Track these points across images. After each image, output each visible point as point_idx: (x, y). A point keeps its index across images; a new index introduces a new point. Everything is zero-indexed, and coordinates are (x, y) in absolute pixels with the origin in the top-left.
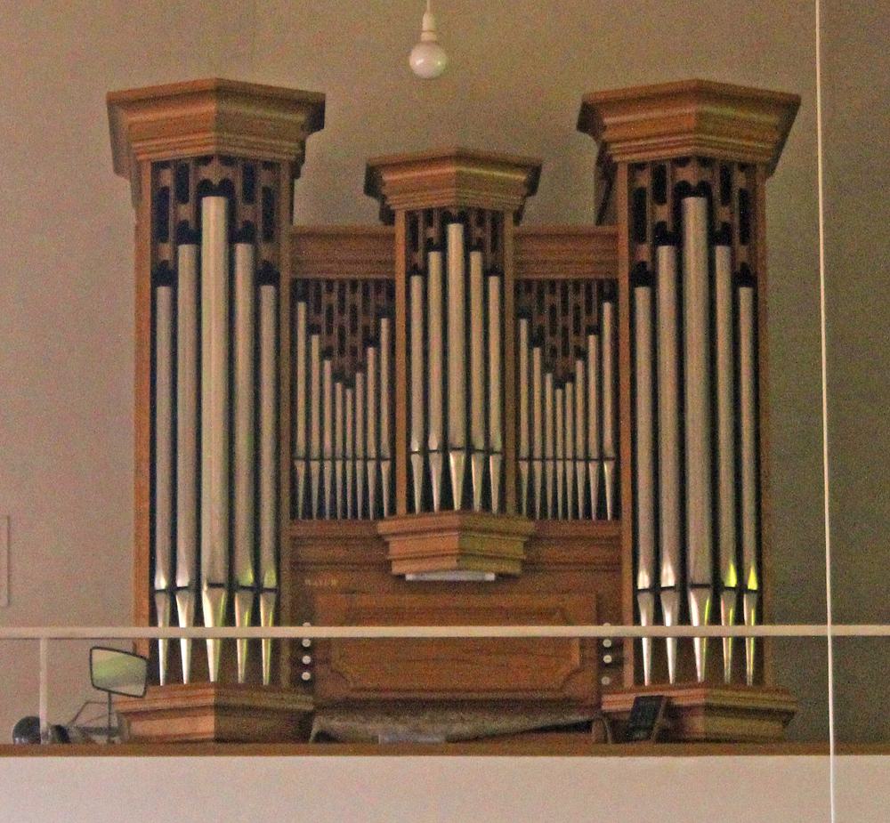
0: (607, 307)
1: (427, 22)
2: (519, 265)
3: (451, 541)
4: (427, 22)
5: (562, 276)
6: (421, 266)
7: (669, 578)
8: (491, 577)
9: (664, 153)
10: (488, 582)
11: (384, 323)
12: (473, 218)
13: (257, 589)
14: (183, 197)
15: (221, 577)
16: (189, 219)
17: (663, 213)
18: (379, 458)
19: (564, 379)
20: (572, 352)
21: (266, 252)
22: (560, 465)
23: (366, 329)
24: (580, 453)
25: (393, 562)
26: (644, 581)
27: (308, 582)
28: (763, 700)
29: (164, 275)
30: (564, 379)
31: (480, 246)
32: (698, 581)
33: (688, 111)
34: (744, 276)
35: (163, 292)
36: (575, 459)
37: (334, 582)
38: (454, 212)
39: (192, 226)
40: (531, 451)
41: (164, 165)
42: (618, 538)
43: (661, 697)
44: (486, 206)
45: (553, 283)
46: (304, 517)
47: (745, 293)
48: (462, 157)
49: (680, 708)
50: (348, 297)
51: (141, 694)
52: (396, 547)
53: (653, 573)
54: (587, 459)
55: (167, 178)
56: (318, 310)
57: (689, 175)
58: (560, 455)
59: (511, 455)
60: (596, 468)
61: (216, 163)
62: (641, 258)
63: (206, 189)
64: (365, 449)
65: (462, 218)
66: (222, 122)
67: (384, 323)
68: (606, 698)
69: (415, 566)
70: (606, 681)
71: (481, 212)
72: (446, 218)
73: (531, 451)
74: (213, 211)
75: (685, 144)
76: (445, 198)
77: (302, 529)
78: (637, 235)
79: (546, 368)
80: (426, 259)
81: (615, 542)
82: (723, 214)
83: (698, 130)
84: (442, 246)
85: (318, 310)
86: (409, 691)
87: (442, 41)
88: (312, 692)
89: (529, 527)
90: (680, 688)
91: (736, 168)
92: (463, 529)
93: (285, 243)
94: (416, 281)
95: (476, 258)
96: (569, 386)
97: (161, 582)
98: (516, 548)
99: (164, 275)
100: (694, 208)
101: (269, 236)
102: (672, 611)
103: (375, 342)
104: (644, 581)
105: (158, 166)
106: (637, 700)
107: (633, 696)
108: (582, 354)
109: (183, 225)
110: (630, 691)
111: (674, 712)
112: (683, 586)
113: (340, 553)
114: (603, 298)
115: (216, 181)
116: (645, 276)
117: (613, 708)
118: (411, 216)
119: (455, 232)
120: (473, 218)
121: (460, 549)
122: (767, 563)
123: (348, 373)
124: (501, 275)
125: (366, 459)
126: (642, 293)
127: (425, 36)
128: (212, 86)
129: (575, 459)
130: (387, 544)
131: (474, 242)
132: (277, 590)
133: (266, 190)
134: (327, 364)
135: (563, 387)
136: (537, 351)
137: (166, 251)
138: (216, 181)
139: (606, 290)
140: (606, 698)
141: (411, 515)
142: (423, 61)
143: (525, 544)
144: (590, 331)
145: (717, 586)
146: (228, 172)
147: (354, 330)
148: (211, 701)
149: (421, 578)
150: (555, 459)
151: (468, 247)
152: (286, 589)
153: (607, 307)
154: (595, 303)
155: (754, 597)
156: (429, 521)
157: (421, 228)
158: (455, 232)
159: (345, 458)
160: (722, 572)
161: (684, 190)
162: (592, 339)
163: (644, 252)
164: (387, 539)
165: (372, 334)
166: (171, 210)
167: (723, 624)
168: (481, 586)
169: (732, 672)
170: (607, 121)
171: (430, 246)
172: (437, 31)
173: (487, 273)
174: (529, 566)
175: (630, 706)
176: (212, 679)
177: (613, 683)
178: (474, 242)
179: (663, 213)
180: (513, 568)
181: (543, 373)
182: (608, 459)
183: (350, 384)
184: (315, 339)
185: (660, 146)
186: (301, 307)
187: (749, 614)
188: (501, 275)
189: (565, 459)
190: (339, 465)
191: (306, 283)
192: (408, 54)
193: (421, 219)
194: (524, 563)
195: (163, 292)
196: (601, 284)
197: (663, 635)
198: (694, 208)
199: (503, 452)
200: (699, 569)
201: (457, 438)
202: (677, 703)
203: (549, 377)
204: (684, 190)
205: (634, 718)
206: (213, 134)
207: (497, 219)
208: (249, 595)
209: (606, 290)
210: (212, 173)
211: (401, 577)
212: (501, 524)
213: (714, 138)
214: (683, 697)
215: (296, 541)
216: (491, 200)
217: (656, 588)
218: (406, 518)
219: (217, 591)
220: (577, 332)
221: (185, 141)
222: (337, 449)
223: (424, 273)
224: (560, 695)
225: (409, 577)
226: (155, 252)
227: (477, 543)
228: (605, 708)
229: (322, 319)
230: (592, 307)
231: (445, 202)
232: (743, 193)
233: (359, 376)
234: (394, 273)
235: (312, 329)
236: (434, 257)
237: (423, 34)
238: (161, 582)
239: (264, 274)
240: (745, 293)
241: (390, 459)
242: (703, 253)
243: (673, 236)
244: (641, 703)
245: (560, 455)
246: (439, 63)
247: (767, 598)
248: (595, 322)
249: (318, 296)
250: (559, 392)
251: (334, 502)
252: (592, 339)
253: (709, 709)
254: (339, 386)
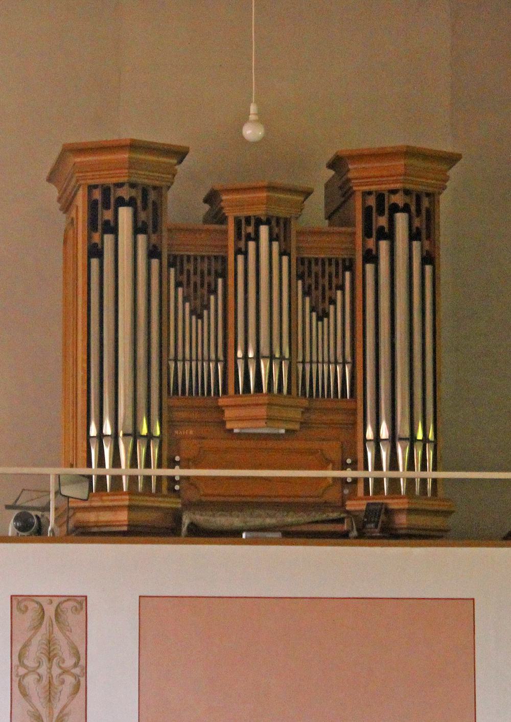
0: (348, 274)
1: (253, 108)
2: (298, 248)
3: (262, 412)
4: (253, 108)
5: (323, 256)
6: (243, 249)
7: (384, 433)
8: (283, 431)
9: (383, 187)
10: (282, 434)
11: (220, 281)
12: (274, 223)
13: (150, 436)
14: (106, 206)
15: (130, 431)
16: (110, 219)
17: (383, 221)
18: (217, 361)
19: (323, 315)
20: (327, 302)
21: (154, 238)
22: (320, 366)
23: (209, 285)
24: (332, 359)
25: (227, 422)
26: (370, 434)
27: (176, 432)
28: (435, 505)
29: (95, 251)
30: (323, 315)
31: (277, 239)
32: (402, 436)
33: (399, 164)
34: (428, 259)
35: (95, 262)
36: (329, 362)
37: (191, 432)
38: (264, 218)
39: (112, 224)
40: (191, 357)
41: (96, 187)
42: (355, 410)
43: (383, 503)
44: (281, 215)
45: (316, 260)
46: (173, 394)
47: (428, 268)
48: (271, 188)
49: (392, 510)
50: (199, 265)
51: (86, 498)
52: (228, 413)
53: (375, 430)
54: (336, 363)
55: (97, 195)
56: (182, 273)
57: (398, 199)
58: (320, 360)
59: (294, 361)
60: (213, 365)
61: (126, 187)
62: (368, 247)
63: (121, 202)
64: (323, 359)
65: (268, 222)
66: (132, 165)
67: (220, 281)
68: (348, 503)
69: (241, 425)
70: (346, 491)
71: (278, 219)
72: (259, 222)
73: (191, 357)
74: (125, 215)
75: (396, 182)
76: (260, 211)
77: (175, 402)
78: (367, 233)
79: (312, 309)
80: (246, 246)
81: (354, 412)
82: (417, 223)
83: (405, 175)
84: (257, 239)
85: (182, 273)
86: (270, 497)
87: (263, 119)
88: (179, 497)
89: (305, 403)
90: (393, 498)
91: (424, 194)
92: (270, 405)
93: (165, 234)
94: (240, 258)
95: (275, 245)
96: (326, 320)
97: (93, 432)
98: (296, 414)
99: (95, 251)
100: (401, 219)
101: (156, 228)
102: (387, 450)
103: (215, 292)
104: (370, 434)
105: (91, 188)
106: (368, 505)
107: (365, 502)
108: (333, 302)
109: (107, 223)
110: (361, 499)
111: (389, 512)
112: (393, 439)
113: (195, 416)
114: (346, 269)
115: (127, 198)
116: (371, 257)
117: (353, 508)
118: (238, 222)
119: (264, 230)
120: (274, 223)
121: (267, 416)
122: (439, 426)
123: (199, 312)
124: (289, 255)
125: (209, 360)
126: (370, 267)
127: (252, 117)
128: (128, 142)
129: (329, 362)
130: (223, 412)
131: (275, 236)
132: (160, 438)
133: (154, 203)
134: (187, 305)
135: (322, 320)
136: (307, 299)
137: (96, 238)
138: (127, 198)
139: (347, 264)
140: (348, 503)
141: (225, 396)
142: (252, 132)
143: (303, 413)
144: (338, 288)
145: (412, 439)
146: (133, 193)
147: (202, 285)
148: (127, 503)
149: (243, 431)
150: (318, 362)
151: (271, 239)
152: (165, 439)
153: (348, 274)
154: (340, 273)
155: (432, 445)
156: (247, 400)
157: (243, 226)
158: (264, 230)
159: (184, 360)
160: (415, 431)
161: (395, 209)
162: (339, 293)
163: (371, 243)
164: (223, 409)
165: (213, 287)
166: (100, 213)
167: (139, 468)
168: (277, 437)
169: (420, 491)
170: (350, 167)
171: (248, 238)
172: (259, 114)
173: (282, 254)
174: (304, 424)
175: (364, 508)
176: (125, 490)
177: (350, 493)
178: (275, 236)
179: (383, 221)
180: (297, 427)
181: (311, 312)
182: (220, 361)
183: (200, 317)
184: (180, 290)
185: (383, 182)
186: (172, 270)
187: (429, 454)
188: (289, 255)
189: (323, 362)
190: (194, 364)
191: (175, 257)
192: (241, 128)
193: (243, 222)
194: (301, 423)
195: (95, 262)
196: (344, 260)
197: (104, 474)
198: (401, 219)
199: (290, 359)
200: (403, 429)
201: (265, 351)
202: (391, 507)
203: (314, 314)
204: (395, 209)
205: (366, 516)
206: (127, 171)
207: (287, 221)
208: (145, 441)
209: (347, 264)
210: (125, 193)
211: (231, 430)
212: (288, 401)
213: (424, 180)
214: (394, 504)
215: (170, 408)
216: (281, 212)
217: (377, 439)
218: (277, 396)
219: (127, 438)
220: (330, 288)
221: (113, 174)
222: (199, 357)
223: (246, 254)
224: (321, 500)
225: (236, 431)
226: (90, 237)
227: (275, 412)
228: (348, 508)
229: (184, 278)
230: (339, 275)
231: (258, 213)
232: (428, 211)
233: (205, 312)
234: (227, 252)
235: (178, 284)
236: (252, 245)
237: (250, 116)
238: (93, 432)
239: (153, 253)
240: (428, 268)
241: (214, 361)
242: (406, 246)
243: (388, 234)
244: (372, 507)
245: (320, 360)
246: (260, 133)
247: (441, 445)
248: (340, 282)
249: (182, 265)
250: (320, 323)
251: (191, 386)
252: (339, 293)
253: (410, 511)
254: (194, 318)
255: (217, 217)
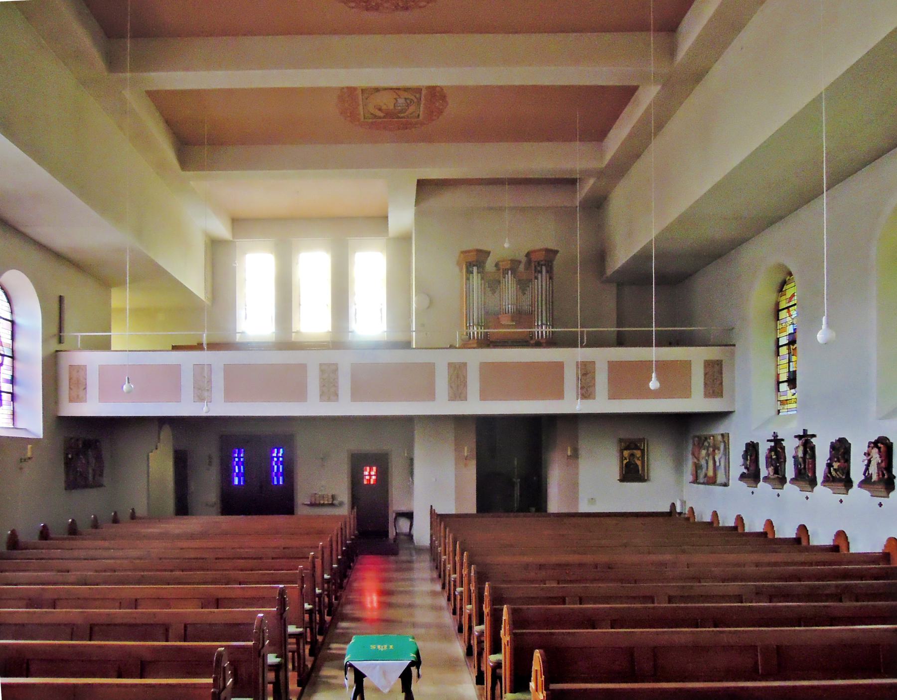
29: (468, 279)
87: (659, 378)
116: (536, 278)
255: (499, 269)
